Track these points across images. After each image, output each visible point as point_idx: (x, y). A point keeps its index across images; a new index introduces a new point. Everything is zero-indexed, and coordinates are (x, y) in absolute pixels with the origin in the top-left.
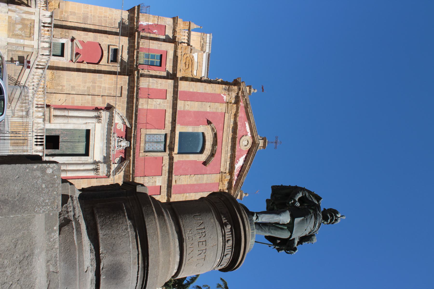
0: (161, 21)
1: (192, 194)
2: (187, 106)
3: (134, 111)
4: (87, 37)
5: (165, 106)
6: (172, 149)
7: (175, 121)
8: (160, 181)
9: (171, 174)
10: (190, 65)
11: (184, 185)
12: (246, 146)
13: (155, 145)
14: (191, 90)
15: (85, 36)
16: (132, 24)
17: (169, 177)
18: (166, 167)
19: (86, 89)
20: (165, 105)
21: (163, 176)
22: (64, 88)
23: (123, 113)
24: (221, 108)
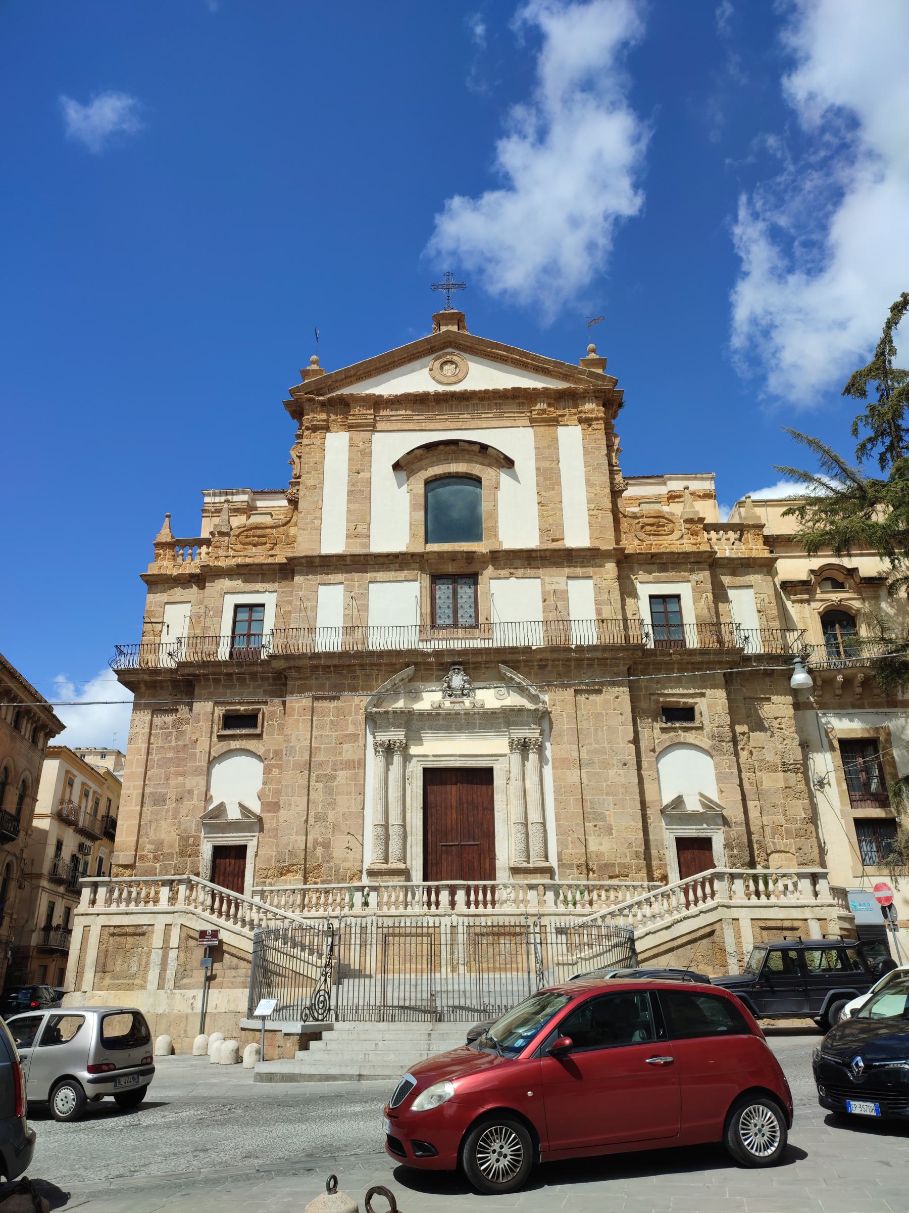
0: (154, 616)
4: (195, 792)
5: (360, 585)
6: (470, 556)
8: (555, 579)
9: (534, 554)
10: (259, 532)
12: (452, 362)
13: (463, 601)
15: (195, 797)
16: (164, 684)
22: (320, 839)
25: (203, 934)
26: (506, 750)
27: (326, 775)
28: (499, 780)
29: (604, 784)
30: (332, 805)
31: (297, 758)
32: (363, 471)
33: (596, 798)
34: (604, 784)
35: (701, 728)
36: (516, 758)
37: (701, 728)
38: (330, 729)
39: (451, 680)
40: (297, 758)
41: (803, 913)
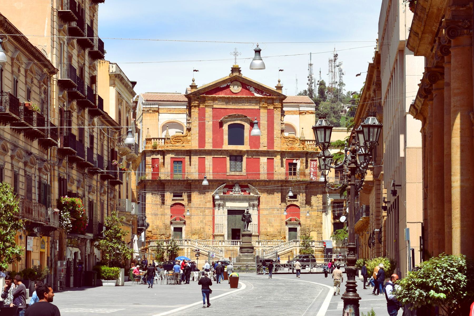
6: (241, 151)
10: (178, 138)
11: (268, 139)
14: (197, 138)
20: (209, 160)
24: (209, 112)
25: (196, 250)
35: (298, 201)
37: (298, 201)
41: (456, 219)
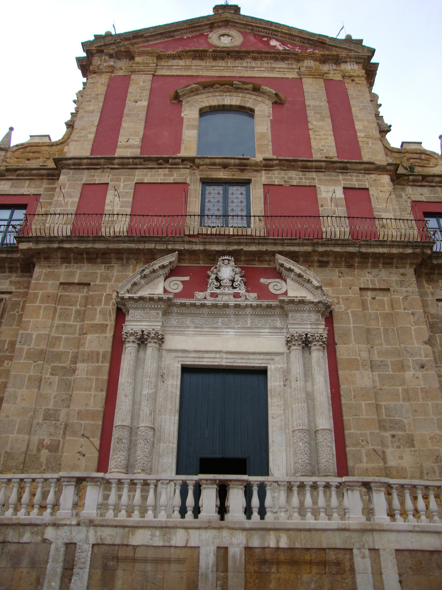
1: (357, 127)
2: (131, 142)
3: (132, 246)
5: (125, 186)
7: (166, 160)
12: (228, 36)
14: (92, 136)
17: (318, 169)
18: (291, 178)
19: (57, 378)
21: (316, 183)
22: (47, 441)
23: (133, 273)
26: (281, 347)
27: (64, 368)
28: (274, 382)
29: (400, 388)
30: (68, 401)
31: (32, 346)
32: (141, 100)
33: (392, 404)
34: (400, 388)
36: (296, 352)
38: (75, 318)
39: (219, 271)
40: (32, 346)
